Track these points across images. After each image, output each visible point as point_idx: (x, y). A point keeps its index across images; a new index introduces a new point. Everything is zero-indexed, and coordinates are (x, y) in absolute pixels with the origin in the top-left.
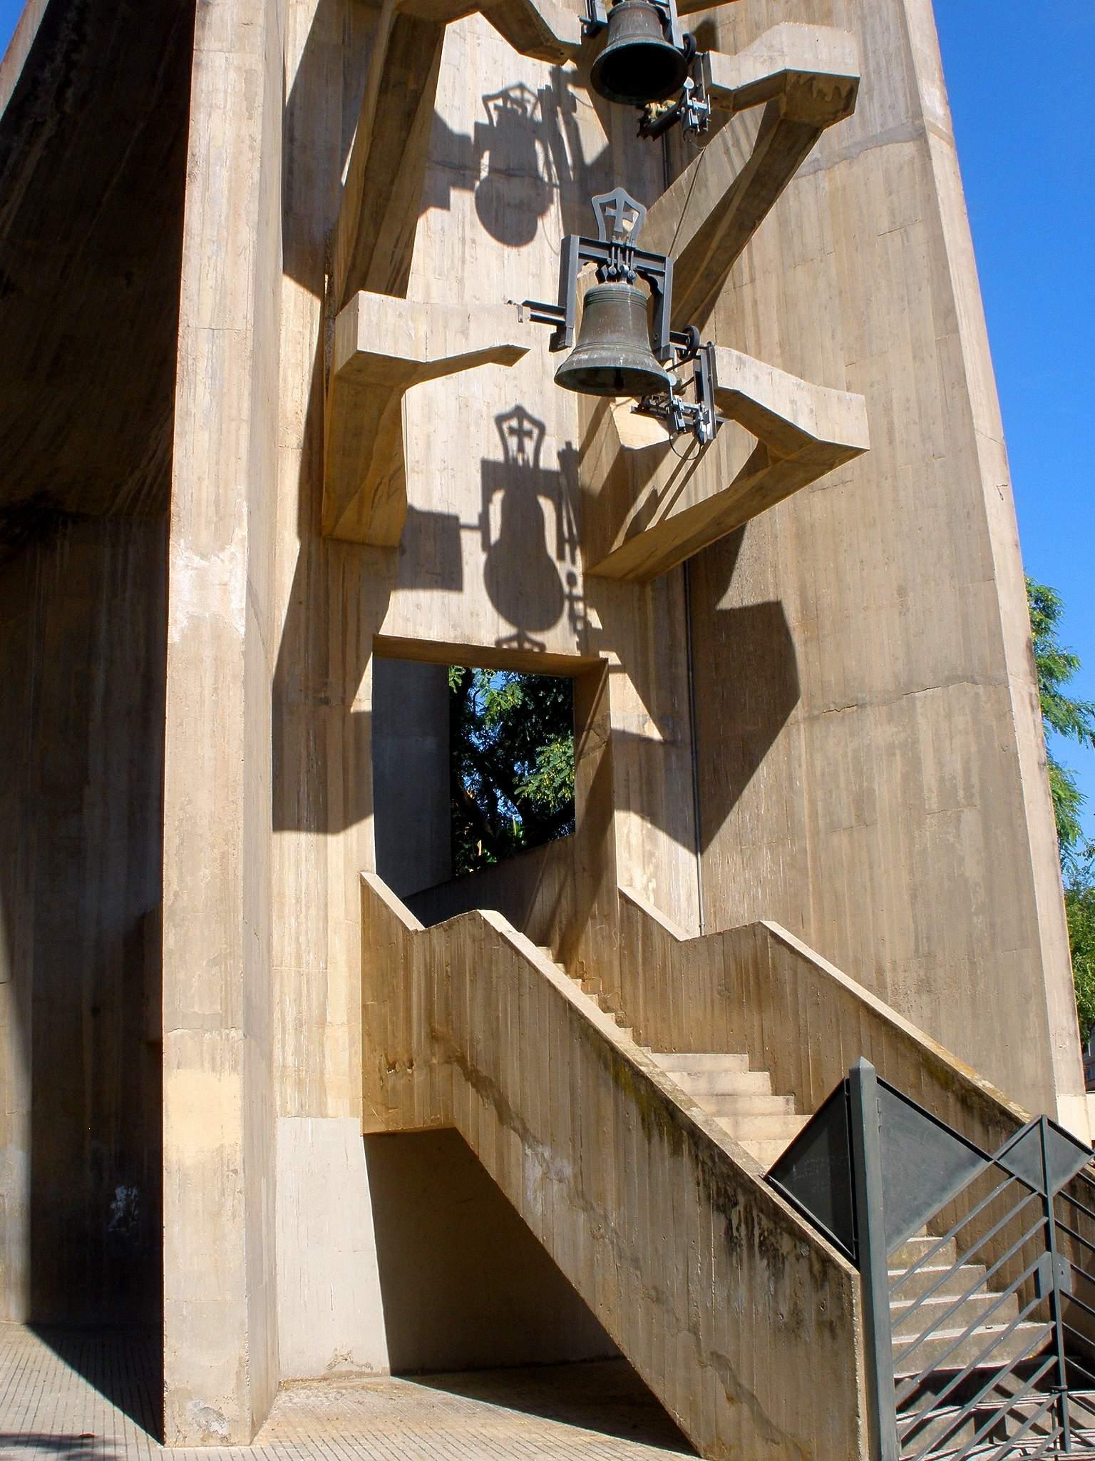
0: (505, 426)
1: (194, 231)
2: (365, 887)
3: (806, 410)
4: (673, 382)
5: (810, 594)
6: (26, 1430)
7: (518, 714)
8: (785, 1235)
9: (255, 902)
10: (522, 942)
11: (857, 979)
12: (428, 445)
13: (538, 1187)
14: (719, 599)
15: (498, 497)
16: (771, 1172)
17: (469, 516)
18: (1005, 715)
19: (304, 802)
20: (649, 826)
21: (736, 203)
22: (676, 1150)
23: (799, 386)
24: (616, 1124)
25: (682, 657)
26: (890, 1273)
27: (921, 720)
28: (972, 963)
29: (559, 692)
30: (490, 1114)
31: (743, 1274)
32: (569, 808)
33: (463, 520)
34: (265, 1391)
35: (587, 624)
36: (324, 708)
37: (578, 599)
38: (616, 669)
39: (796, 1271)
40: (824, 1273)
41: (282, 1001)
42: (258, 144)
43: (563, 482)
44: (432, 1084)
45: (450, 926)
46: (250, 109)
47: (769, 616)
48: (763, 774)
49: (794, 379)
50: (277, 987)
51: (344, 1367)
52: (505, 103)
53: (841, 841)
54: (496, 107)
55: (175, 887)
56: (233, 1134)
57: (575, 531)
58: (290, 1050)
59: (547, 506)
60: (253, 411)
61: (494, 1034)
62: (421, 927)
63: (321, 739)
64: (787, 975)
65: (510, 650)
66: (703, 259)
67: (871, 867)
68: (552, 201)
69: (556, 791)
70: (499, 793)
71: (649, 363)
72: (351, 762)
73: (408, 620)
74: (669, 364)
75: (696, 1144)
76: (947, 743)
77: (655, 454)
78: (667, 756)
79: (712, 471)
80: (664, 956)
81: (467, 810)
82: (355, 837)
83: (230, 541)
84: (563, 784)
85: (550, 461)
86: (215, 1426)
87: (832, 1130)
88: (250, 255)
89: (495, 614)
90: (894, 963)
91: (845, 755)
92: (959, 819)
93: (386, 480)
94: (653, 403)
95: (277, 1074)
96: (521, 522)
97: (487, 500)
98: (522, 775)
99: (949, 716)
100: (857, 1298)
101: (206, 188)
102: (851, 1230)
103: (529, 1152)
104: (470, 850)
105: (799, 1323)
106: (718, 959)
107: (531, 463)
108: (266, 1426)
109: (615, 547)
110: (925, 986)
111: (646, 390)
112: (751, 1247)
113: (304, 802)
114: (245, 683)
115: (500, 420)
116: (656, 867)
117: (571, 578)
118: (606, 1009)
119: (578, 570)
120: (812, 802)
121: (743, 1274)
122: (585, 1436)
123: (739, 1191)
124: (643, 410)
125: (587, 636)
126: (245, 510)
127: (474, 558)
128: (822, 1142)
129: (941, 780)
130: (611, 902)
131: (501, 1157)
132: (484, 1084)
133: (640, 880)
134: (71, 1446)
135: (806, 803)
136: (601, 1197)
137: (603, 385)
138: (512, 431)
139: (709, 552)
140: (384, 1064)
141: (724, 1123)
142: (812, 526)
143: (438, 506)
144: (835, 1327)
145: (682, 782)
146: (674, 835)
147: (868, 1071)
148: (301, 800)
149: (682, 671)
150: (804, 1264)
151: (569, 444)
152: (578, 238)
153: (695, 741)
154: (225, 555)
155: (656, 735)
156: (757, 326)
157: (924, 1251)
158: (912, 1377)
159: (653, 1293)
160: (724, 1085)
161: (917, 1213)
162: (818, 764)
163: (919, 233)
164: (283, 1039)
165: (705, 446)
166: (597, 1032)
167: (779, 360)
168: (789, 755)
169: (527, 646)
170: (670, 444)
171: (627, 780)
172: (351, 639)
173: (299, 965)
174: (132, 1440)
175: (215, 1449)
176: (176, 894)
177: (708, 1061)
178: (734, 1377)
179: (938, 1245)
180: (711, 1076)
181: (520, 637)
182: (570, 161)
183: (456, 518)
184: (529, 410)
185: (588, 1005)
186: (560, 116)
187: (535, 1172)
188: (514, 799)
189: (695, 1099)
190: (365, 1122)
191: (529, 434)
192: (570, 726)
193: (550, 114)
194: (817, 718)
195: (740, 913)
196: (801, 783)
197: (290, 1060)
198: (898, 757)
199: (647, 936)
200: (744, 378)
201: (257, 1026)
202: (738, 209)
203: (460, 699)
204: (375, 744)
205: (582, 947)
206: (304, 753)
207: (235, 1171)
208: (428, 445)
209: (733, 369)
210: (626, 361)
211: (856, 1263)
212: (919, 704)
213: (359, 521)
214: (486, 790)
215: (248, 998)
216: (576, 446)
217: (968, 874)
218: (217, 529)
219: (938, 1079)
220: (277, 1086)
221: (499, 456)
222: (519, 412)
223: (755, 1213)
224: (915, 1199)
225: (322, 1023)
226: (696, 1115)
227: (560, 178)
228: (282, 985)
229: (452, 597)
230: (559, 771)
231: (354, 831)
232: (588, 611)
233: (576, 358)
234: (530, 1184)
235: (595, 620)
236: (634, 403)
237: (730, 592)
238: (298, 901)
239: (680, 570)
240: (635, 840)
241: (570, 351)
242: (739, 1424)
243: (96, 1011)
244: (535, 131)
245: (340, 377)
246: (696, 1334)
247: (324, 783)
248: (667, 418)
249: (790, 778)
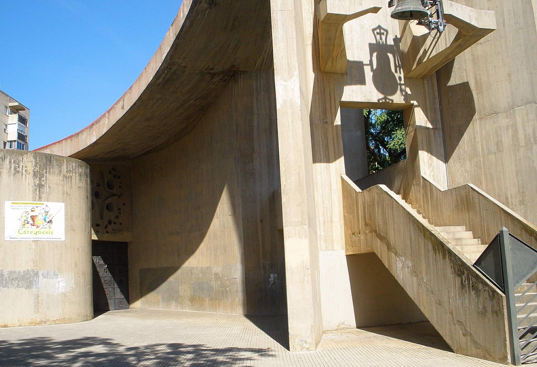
0: (375, 32)
2: (342, 179)
3: (474, 18)
4: (429, 13)
5: (478, 78)
6: (248, 347)
7: (387, 122)
8: (480, 284)
9: (308, 185)
10: (392, 194)
11: (499, 201)
13: (401, 270)
15: (375, 54)
16: (475, 264)
17: (366, 61)
22: (444, 257)
23: (471, 10)
24: (425, 250)
25: (437, 101)
26: (515, 295)
27: (517, 117)
29: (398, 115)
30: (385, 248)
31: (467, 295)
32: (404, 151)
33: (364, 63)
34: (320, 333)
35: (406, 93)
36: (326, 125)
37: (403, 85)
38: (416, 106)
39: (484, 295)
40: (493, 295)
43: (395, 49)
44: (366, 239)
45: (370, 190)
47: (465, 86)
48: (466, 136)
49: (469, 8)
50: (317, 211)
51: (342, 326)
53: (492, 157)
56: (307, 257)
58: (322, 230)
59: (390, 56)
60: (297, 35)
61: (385, 223)
62: (361, 191)
63: (326, 134)
64: (477, 200)
65: (383, 102)
67: (502, 165)
69: (400, 145)
70: (381, 147)
71: (421, 8)
72: (336, 141)
74: (427, 8)
75: (450, 255)
76: (527, 124)
77: (425, 37)
78: (434, 133)
79: (443, 41)
80: (437, 197)
81: (372, 153)
84: (402, 143)
85: (390, 42)
86: (305, 345)
87: (495, 250)
91: (492, 130)
92: (532, 148)
93: (340, 53)
94: (423, 21)
95: (318, 238)
96: (383, 62)
97: (371, 56)
98: (388, 141)
99: (527, 115)
100: (505, 303)
102: (502, 281)
103: (397, 259)
104: (373, 165)
105: (486, 311)
106: (454, 196)
108: (320, 345)
109: (413, 68)
110: (522, 202)
111: (420, 17)
112: (469, 287)
114: (302, 119)
115: (373, 30)
116: (433, 168)
117: (400, 78)
118: (419, 213)
119: (402, 76)
120: (482, 145)
121: (467, 295)
122: (419, 346)
123: (465, 270)
124: (420, 23)
125: (406, 96)
126: (297, 66)
127: (369, 74)
128: (491, 254)
129: (526, 136)
130: (419, 180)
131: (389, 261)
132: (383, 238)
133: (428, 173)
134: (262, 352)
136: (421, 272)
137: (407, 17)
138: (377, 33)
139: (444, 67)
140: (352, 233)
141: (458, 248)
142: (478, 56)
144: (498, 313)
145: (440, 141)
146: (438, 158)
147: (506, 231)
148: (321, 153)
150: (487, 292)
151: (396, 36)
155: (430, 126)
157: (526, 288)
158: (524, 329)
159: (438, 302)
160: (458, 236)
161: (524, 276)
162: (484, 133)
164: (320, 227)
165: (441, 33)
166: (418, 221)
167: (464, 3)
168: (474, 131)
169: (387, 101)
170: (430, 33)
171: (422, 141)
172: (333, 101)
174: (280, 350)
175: (305, 352)
176: (285, 185)
177: (452, 228)
178: (465, 328)
179: (532, 286)
180: (454, 233)
181: (385, 98)
183: (362, 62)
184: (383, 26)
185: (413, 212)
187: (400, 265)
188: (386, 149)
189: (449, 241)
190: (347, 250)
191: (383, 34)
192: (403, 125)
194: (482, 118)
195: (460, 182)
196: (478, 139)
197: (322, 233)
199: (431, 190)
201: (311, 223)
203: (367, 118)
204: (342, 135)
205: (411, 194)
207: (308, 269)
210: (413, 8)
211: (504, 292)
212: (517, 112)
213: (332, 66)
214: (377, 147)
215: (309, 215)
216: (399, 36)
218: (289, 72)
219: (528, 233)
220: (318, 242)
222: (379, 27)
223: (470, 277)
225: (332, 222)
226: (450, 246)
229: (363, 87)
230: (400, 139)
233: (397, 9)
234: (398, 269)
236: (416, 21)
237: (452, 79)
238: (322, 184)
239: (435, 74)
240: (426, 160)
241: (395, 7)
242: (467, 343)
243: (261, 221)
245: (322, 22)
246: (452, 315)
247: (327, 147)
248: (428, 25)
249: (475, 138)
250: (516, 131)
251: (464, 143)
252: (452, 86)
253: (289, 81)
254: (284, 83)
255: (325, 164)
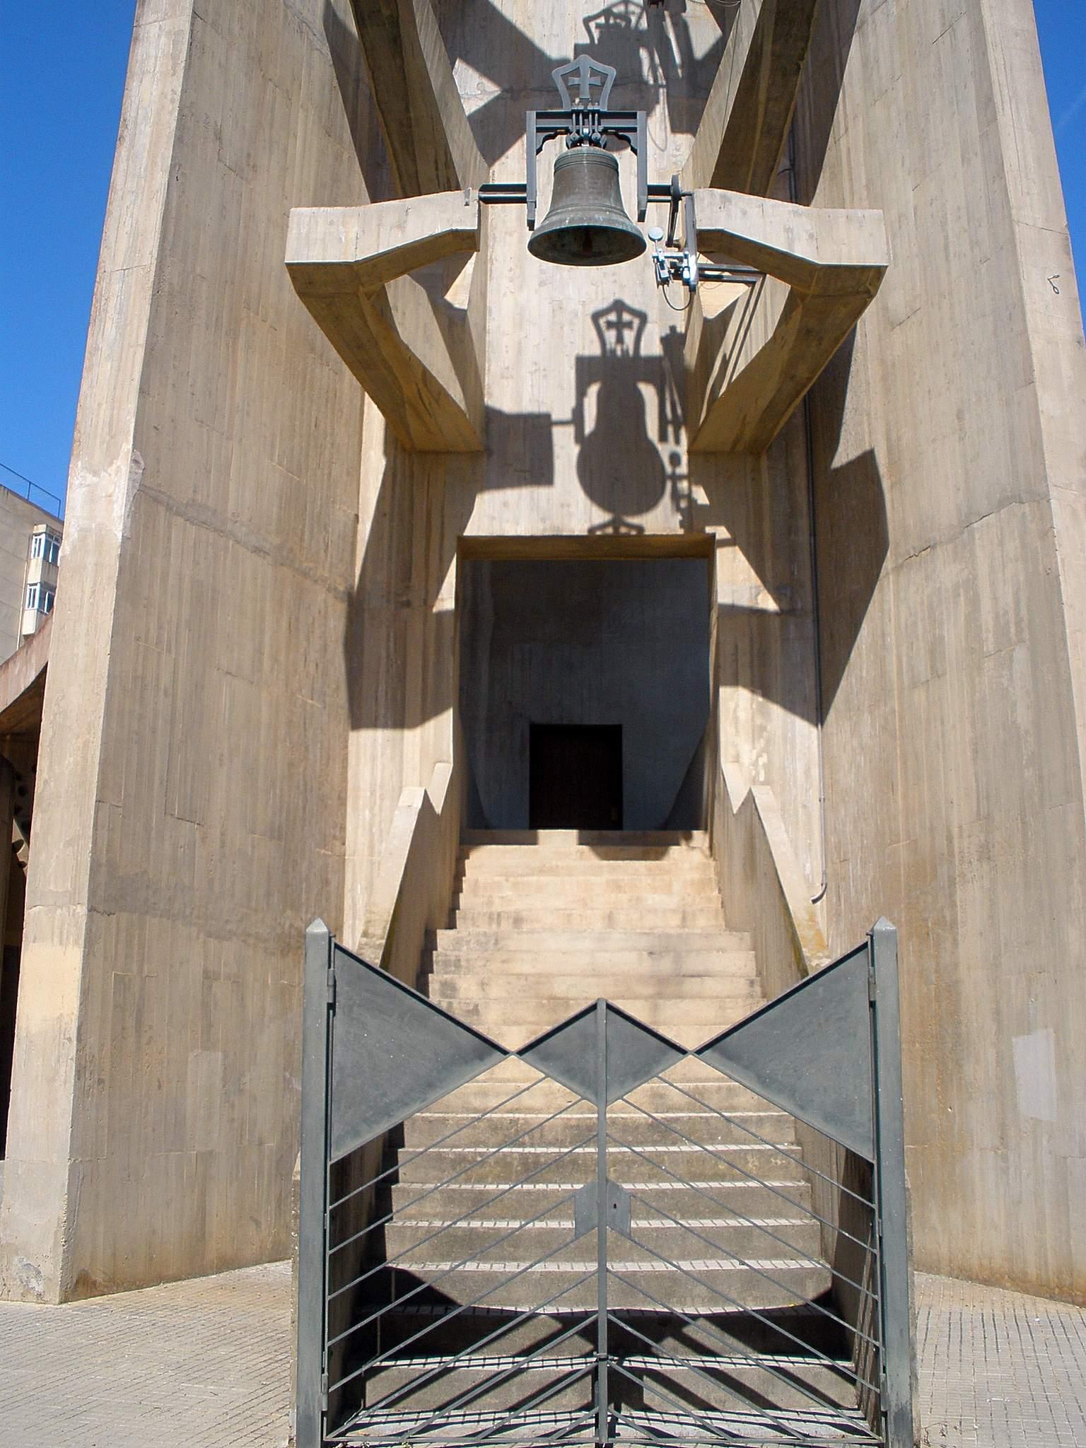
0: (602, 321)
1: (118, 187)
3: (805, 236)
5: (894, 436)
12: (519, 351)
14: (832, 458)
15: (594, 390)
17: (561, 409)
18: (1046, 534)
19: (382, 700)
20: (761, 699)
21: (768, 47)
25: (804, 523)
27: (979, 553)
28: (1024, 823)
33: (554, 417)
36: (406, 611)
37: (681, 477)
38: (725, 543)
41: (353, 889)
42: (178, 97)
46: (174, 68)
52: (607, 20)
53: (920, 696)
54: (598, 26)
55: (45, 776)
57: (679, 411)
59: (648, 392)
66: (756, 115)
67: (943, 723)
68: (658, 102)
72: (432, 659)
73: (493, 518)
79: (761, 327)
82: (432, 731)
83: (115, 457)
85: (652, 347)
88: (161, 197)
89: (588, 502)
90: (960, 827)
93: (421, 386)
96: (620, 412)
99: (1001, 543)
101: (132, 146)
107: (631, 352)
113: (382, 700)
115: (596, 317)
116: (768, 742)
117: (675, 459)
125: (692, 515)
127: (566, 449)
129: (997, 617)
135: (894, 658)
138: (610, 325)
142: (894, 365)
143: (528, 407)
146: (790, 707)
149: (804, 538)
151: (673, 329)
152: (534, 113)
153: (817, 609)
154: (112, 469)
155: (768, 603)
156: (850, 173)
163: (963, 26)
164: (354, 924)
169: (623, 530)
171: (736, 653)
173: (371, 854)
175: (33, 1306)
176: (46, 782)
181: (615, 523)
182: (678, 60)
183: (548, 416)
184: (628, 302)
186: (668, 20)
193: (656, 22)
196: (891, 640)
198: (962, 598)
200: (729, 216)
202: (773, 54)
206: (384, 654)
207: (70, 1039)
208: (519, 351)
209: (716, 208)
212: (977, 536)
217: (1019, 720)
221: (595, 350)
222: (619, 306)
224: (385, 1095)
227: (666, 78)
228: (354, 874)
229: (542, 492)
231: (431, 725)
232: (694, 489)
235: (701, 496)
237: (841, 448)
238: (373, 793)
240: (743, 715)
244: (640, 38)
247: (402, 678)
249: (883, 635)
250: (974, 603)
251: (860, 655)
252: (842, 467)
253: (103, 474)
254: (90, 479)
255: (389, 733)
